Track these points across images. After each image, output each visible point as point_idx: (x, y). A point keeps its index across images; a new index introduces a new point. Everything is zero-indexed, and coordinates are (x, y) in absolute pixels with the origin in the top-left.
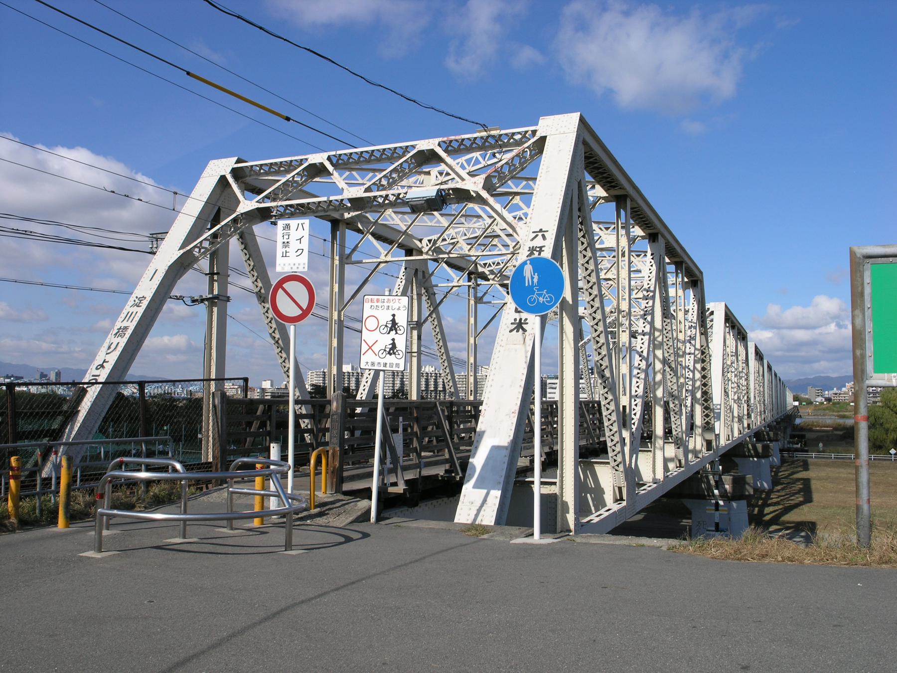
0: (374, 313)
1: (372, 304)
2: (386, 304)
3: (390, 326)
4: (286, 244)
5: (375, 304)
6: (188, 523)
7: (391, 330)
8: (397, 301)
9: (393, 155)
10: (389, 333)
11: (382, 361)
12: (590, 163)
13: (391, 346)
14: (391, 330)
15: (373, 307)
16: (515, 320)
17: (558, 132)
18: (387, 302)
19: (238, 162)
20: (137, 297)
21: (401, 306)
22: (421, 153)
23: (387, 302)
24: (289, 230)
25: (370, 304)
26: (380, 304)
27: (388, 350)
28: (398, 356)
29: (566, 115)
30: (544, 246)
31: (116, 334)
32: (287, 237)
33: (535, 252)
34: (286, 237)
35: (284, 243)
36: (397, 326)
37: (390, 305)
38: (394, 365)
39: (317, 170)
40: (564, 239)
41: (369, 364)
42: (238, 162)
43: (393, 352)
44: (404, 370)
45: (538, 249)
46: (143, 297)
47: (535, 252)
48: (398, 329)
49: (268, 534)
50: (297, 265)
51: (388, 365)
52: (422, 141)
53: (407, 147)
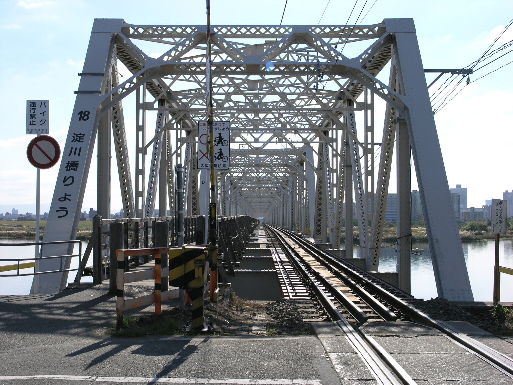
3: (218, 140)
8: (222, 124)
10: (217, 145)
12: (120, 52)
13: (219, 154)
14: (219, 143)
15: (205, 129)
21: (225, 127)
25: (203, 127)
27: (217, 156)
36: (222, 141)
37: (218, 127)
38: (222, 166)
40: (250, 270)
41: (204, 166)
43: (221, 157)
48: (223, 142)
49: (66, 354)
51: (217, 166)
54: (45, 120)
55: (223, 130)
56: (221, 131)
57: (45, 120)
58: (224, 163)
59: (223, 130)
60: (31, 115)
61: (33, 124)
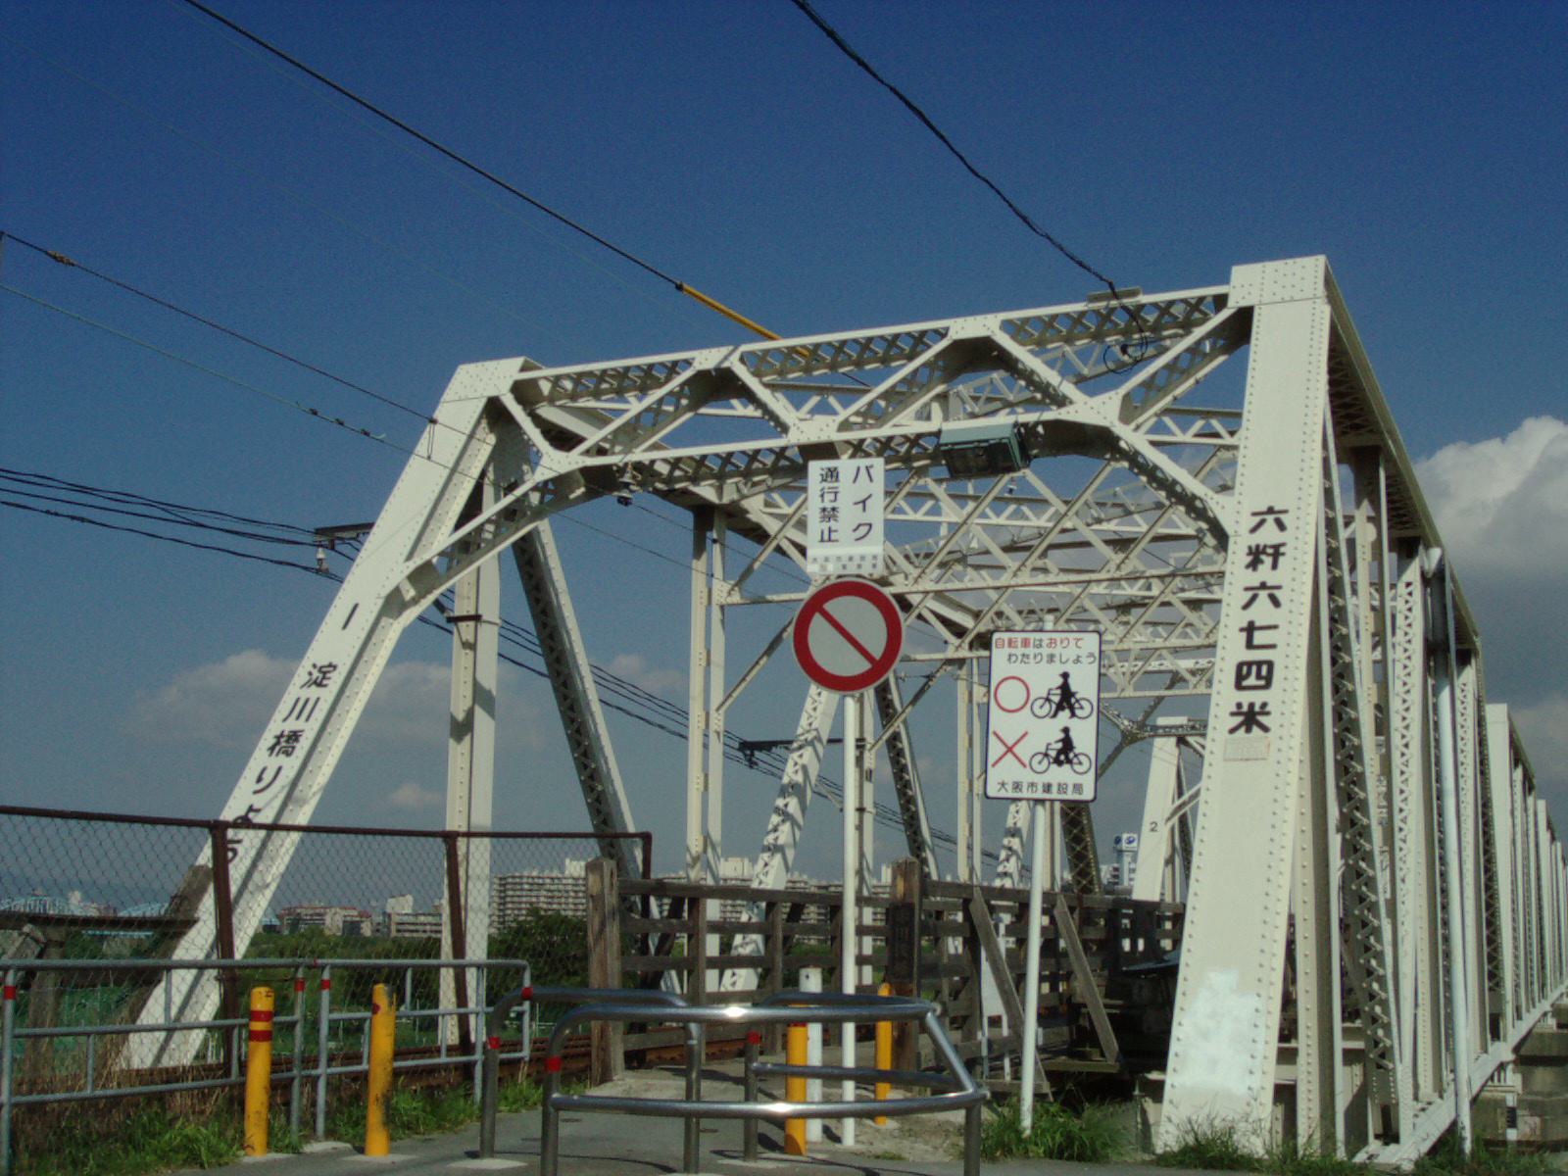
0: (1017, 669)
1: (1013, 651)
2: (1045, 651)
3: (1056, 699)
4: (829, 514)
5: (1020, 651)
6: (705, 1123)
7: (1060, 707)
8: (1072, 643)
9: (892, 350)
10: (1055, 715)
11: (1041, 780)
13: (1060, 745)
14: (1060, 707)
15: (1013, 658)
16: (1239, 705)
17: (1278, 298)
18: (1049, 645)
19: (523, 369)
20: (314, 666)
21: (1083, 653)
22: (959, 346)
23: (1049, 645)
24: (837, 480)
25: (1007, 650)
26: (1031, 651)
27: (1053, 754)
28: (1077, 767)
29: (1290, 261)
30: (1283, 544)
31: (272, 749)
32: (832, 497)
33: (1263, 557)
34: (829, 497)
35: (824, 510)
36: (1073, 700)
37: (1057, 651)
39: (719, 385)
41: (1009, 787)
42: (523, 369)
43: (1067, 758)
44: (1092, 801)
45: (1270, 551)
46: (330, 665)
47: (1263, 557)
48: (1077, 705)
50: (857, 561)
51: (1055, 789)
52: (960, 321)
53: (923, 333)
54: (870, 525)
55: (1077, 660)
56: (1069, 668)
57: (870, 525)
58: (1078, 779)
59: (1077, 660)
60: (824, 510)
61: (830, 540)
